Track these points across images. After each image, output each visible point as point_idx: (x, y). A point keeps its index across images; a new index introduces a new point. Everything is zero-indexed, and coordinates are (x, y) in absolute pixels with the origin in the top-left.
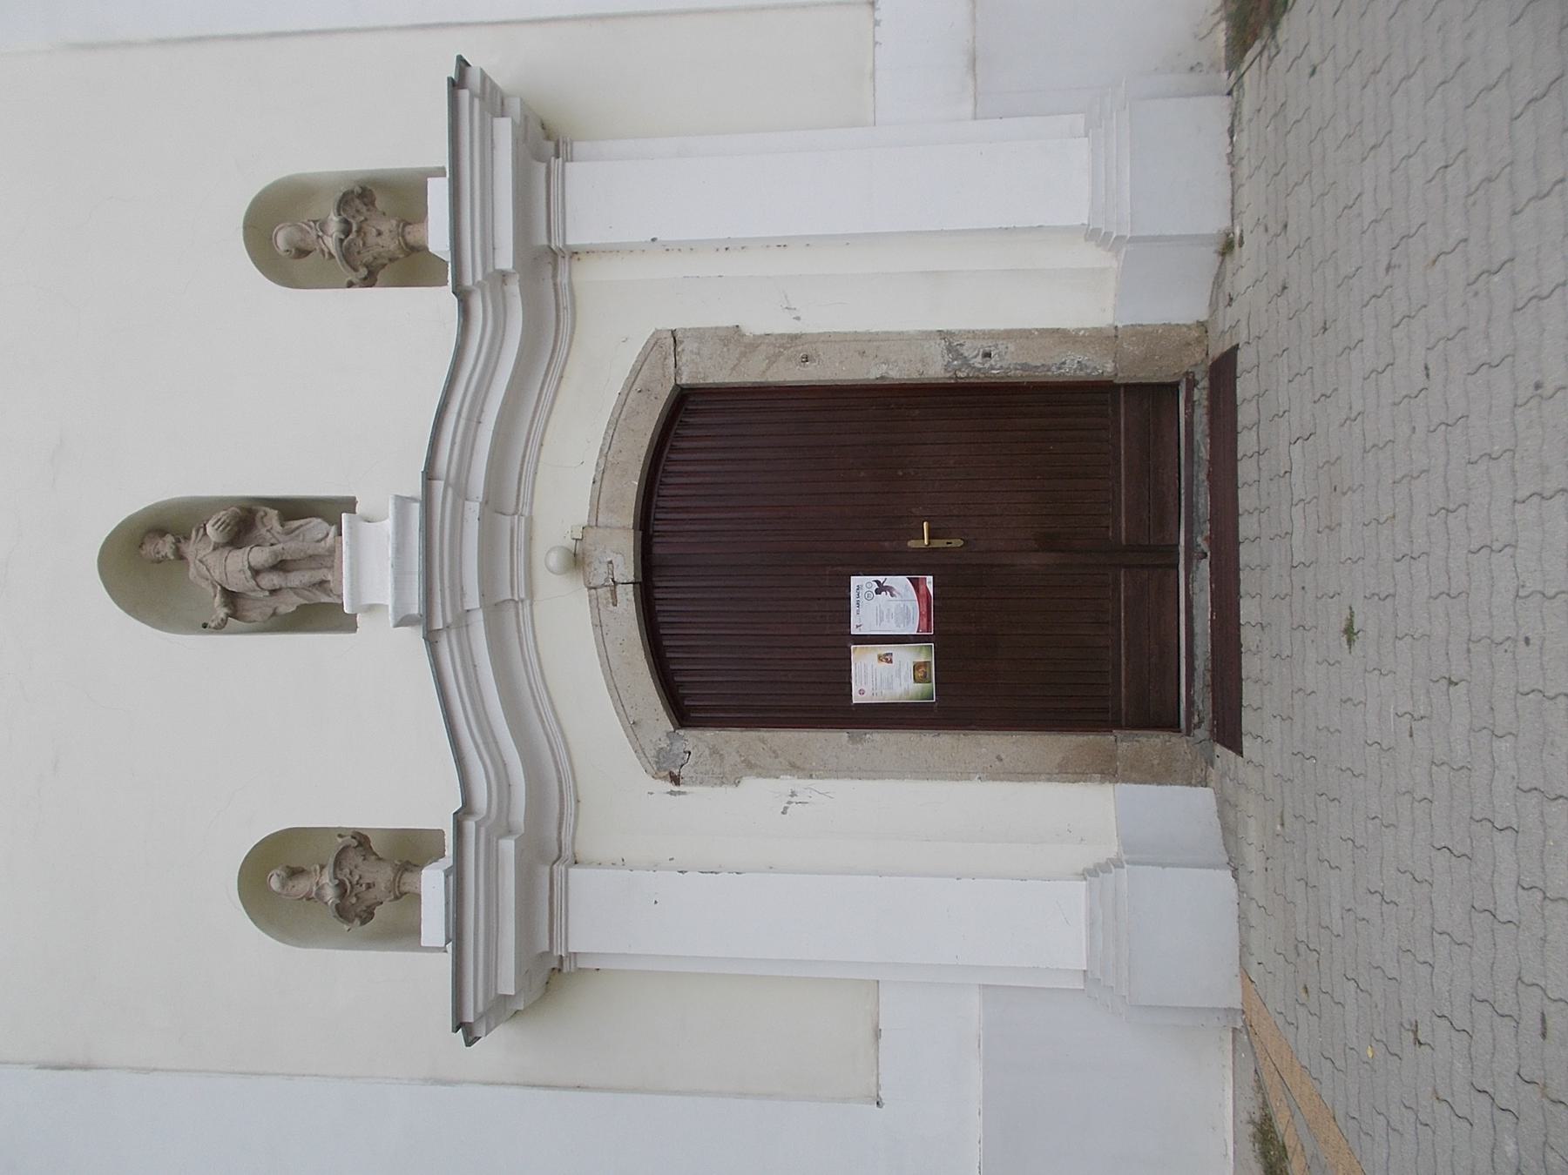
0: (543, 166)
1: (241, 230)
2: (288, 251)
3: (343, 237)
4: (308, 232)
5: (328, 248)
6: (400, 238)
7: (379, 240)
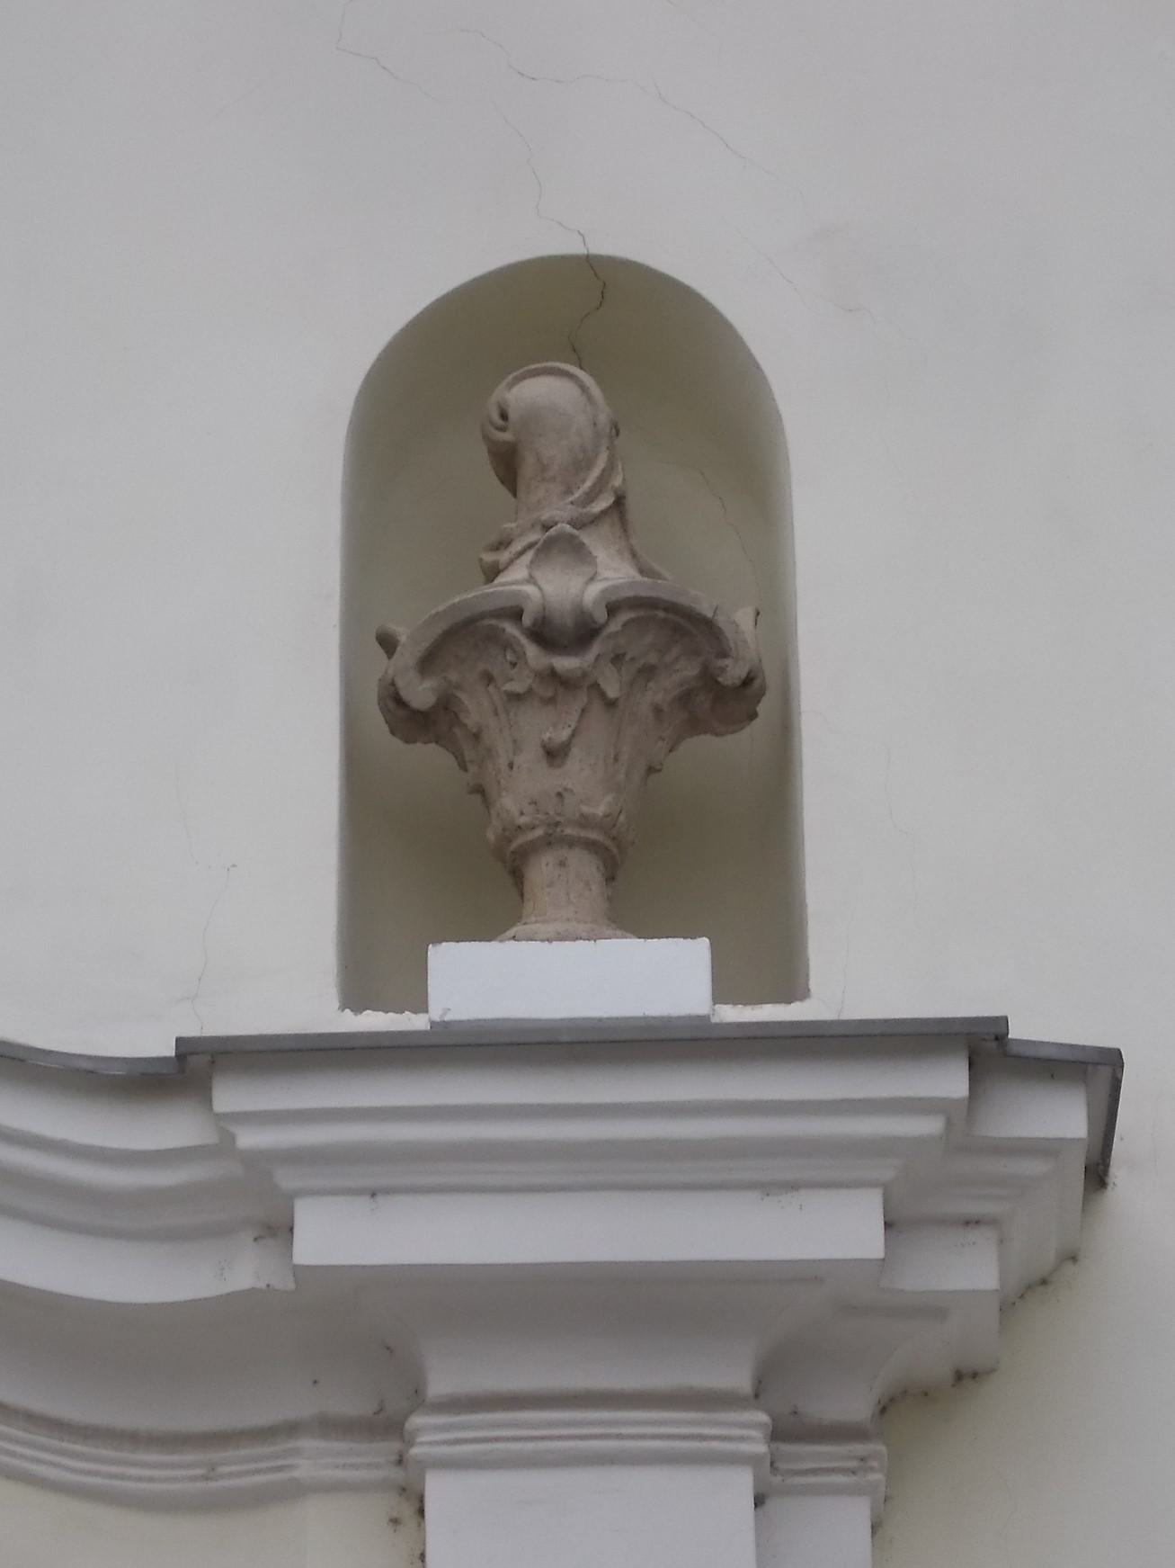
0: (739, 1378)
1: (574, 247)
2: (504, 416)
3: (527, 620)
4: (569, 491)
5: (511, 562)
6: (539, 832)
7: (530, 757)
